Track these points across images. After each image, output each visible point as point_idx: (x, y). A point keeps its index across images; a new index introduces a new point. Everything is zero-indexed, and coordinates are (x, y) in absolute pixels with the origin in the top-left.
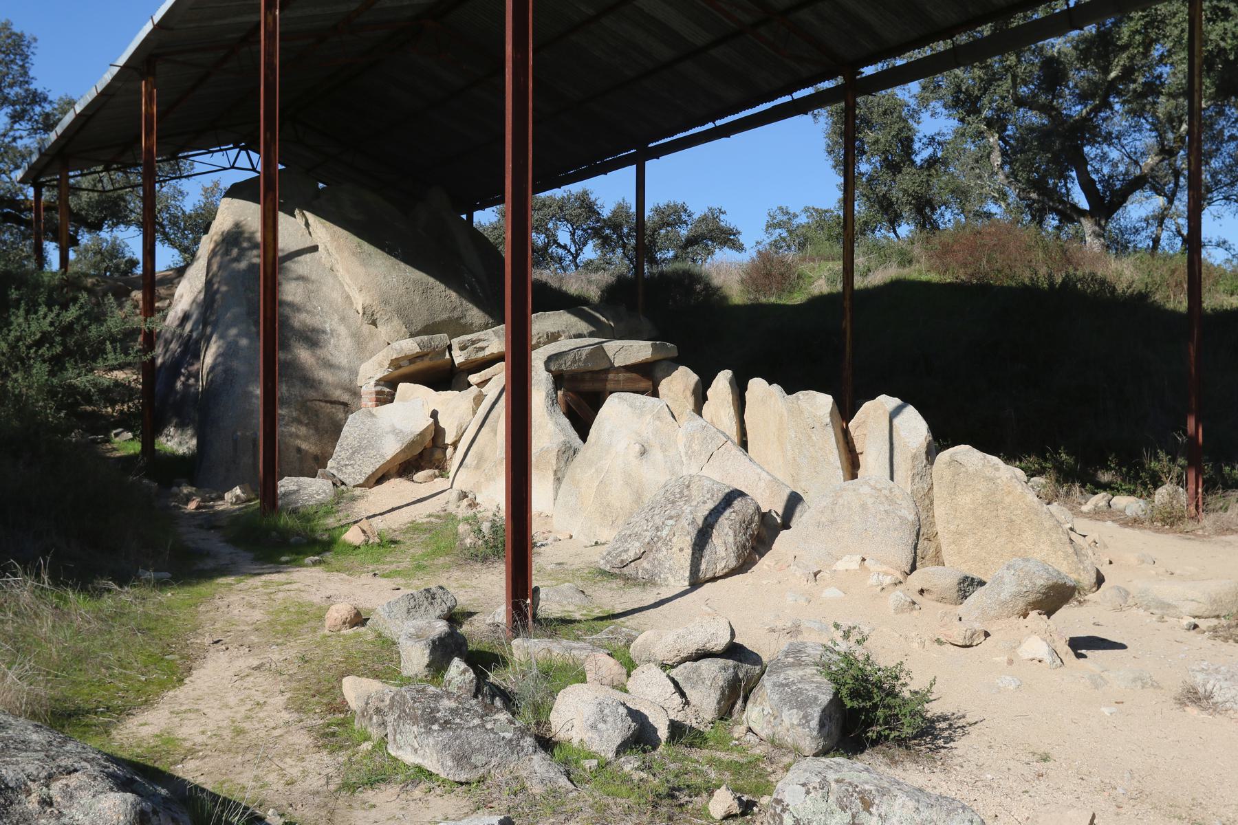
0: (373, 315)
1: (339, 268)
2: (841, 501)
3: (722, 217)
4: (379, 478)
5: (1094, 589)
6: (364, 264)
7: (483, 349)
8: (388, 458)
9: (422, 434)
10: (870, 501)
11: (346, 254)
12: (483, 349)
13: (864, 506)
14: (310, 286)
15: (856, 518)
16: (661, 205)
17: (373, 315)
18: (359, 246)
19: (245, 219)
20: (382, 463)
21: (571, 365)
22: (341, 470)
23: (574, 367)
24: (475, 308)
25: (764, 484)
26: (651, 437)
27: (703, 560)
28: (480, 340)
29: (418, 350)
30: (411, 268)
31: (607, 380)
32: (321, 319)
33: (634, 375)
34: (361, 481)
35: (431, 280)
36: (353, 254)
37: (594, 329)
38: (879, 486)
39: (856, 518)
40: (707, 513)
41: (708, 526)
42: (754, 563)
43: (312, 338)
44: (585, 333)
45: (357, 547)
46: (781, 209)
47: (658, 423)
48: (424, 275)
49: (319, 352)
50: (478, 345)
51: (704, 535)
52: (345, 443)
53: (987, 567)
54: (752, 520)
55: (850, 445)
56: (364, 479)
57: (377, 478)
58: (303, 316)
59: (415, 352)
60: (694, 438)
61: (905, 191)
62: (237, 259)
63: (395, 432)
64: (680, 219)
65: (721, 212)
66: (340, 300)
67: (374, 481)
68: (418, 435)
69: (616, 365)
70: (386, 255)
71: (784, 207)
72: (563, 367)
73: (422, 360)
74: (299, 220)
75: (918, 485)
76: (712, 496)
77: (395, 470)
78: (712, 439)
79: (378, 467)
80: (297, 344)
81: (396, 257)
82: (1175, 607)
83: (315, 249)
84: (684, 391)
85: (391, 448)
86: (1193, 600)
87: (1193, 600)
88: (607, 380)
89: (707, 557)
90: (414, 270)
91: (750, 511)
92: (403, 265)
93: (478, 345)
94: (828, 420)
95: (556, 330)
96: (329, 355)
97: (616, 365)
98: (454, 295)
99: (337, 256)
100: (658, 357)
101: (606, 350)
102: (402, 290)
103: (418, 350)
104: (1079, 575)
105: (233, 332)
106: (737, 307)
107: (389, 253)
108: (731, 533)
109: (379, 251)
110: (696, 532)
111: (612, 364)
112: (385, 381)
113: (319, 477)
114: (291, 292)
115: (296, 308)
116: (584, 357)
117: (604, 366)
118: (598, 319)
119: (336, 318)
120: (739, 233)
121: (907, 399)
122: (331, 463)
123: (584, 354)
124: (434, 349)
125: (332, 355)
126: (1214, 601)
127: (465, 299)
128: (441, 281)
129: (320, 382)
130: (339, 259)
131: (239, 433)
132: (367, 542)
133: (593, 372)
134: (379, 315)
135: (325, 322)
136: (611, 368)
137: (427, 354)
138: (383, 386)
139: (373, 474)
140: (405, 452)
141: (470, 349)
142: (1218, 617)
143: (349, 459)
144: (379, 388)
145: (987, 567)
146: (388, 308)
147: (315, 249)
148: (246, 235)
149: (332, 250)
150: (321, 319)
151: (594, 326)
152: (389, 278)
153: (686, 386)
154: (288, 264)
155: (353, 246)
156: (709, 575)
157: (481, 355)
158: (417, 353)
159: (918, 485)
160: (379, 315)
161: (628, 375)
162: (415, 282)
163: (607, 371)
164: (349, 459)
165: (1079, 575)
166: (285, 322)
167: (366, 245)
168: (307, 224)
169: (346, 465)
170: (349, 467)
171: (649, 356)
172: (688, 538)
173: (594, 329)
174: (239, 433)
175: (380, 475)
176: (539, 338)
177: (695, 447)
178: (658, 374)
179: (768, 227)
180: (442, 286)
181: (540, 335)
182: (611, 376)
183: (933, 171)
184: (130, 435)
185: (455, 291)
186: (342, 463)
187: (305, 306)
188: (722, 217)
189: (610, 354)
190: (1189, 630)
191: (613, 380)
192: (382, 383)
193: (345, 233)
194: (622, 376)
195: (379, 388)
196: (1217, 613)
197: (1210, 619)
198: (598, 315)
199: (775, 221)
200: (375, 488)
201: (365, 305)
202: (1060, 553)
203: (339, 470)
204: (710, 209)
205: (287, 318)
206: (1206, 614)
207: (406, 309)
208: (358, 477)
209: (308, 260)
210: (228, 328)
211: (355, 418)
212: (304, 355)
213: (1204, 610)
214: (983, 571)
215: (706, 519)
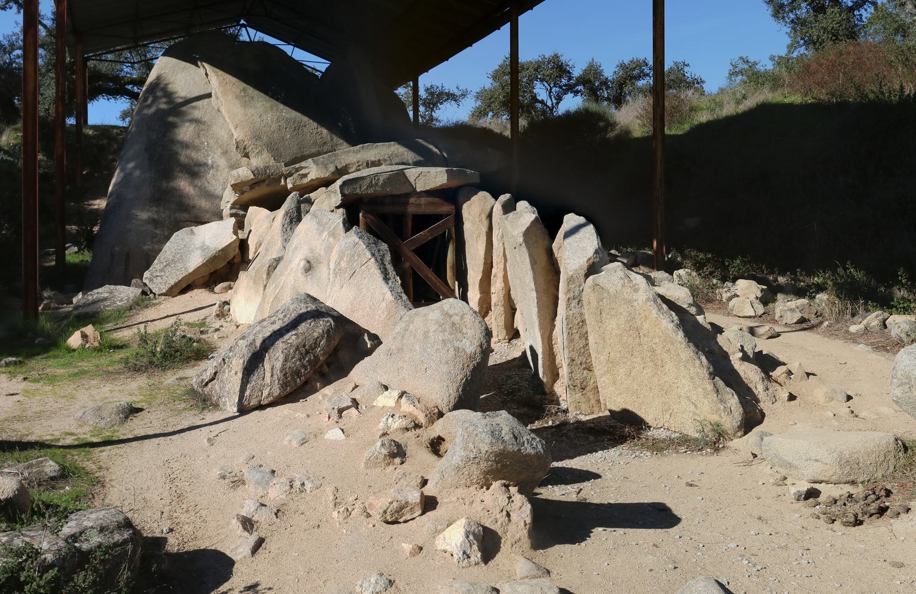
0: (245, 149)
1: (223, 110)
2: (411, 327)
3: (686, 69)
4: (184, 287)
5: (739, 434)
6: (245, 105)
7: (305, 175)
8: (191, 271)
9: (224, 250)
10: (433, 328)
11: (230, 97)
12: (305, 175)
13: (426, 334)
14: (201, 126)
15: (417, 348)
16: (626, 62)
17: (245, 149)
18: (244, 90)
19: (165, 73)
20: (184, 275)
21: (367, 189)
22: (152, 280)
23: (371, 191)
24: (345, 143)
25: (385, 305)
26: (322, 253)
27: (248, 386)
28: (302, 168)
29: (252, 177)
30: (288, 108)
31: (408, 204)
32: (206, 153)
33: (436, 199)
34: (164, 291)
35: (305, 119)
36: (237, 97)
37: (421, 159)
38: (451, 312)
39: (417, 348)
40: (268, 334)
41: (264, 348)
42: (314, 391)
43: (194, 171)
44: (410, 162)
45: (74, 350)
46: (741, 58)
47: (331, 239)
48: (299, 115)
49: (198, 182)
50: (301, 172)
51: (256, 359)
52: (163, 257)
53: (640, 401)
54: (316, 343)
55: (556, 266)
56: (167, 288)
57: (181, 289)
58: (188, 152)
59: (250, 178)
60: (344, 255)
61: (825, 29)
62: (149, 106)
63: (203, 248)
64: (642, 71)
65: (685, 65)
66: (226, 137)
67: (178, 291)
68: (220, 251)
69: (418, 190)
70: (267, 98)
71: (744, 57)
72: (358, 191)
73: (260, 186)
74: (202, 71)
75: (574, 311)
76: (285, 316)
77: (201, 281)
78: (359, 256)
79: (180, 278)
80: (180, 174)
81: (277, 100)
82: (796, 468)
83: (209, 96)
84: (480, 215)
85: (195, 261)
86: (817, 461)
87: (817, 461)
88: (408, 204)
89: (253, 383)
90: (291, 110)
91: (316, 335)
92: (281, 106)
93: (301, 172)
94: (521, 240)
95: (377, 159)
96: (206, 183)
97: (418, 190)
98: (325, 131)
99: (222, 99)
100: (455, 183)
101: (408, 176)
102: (274, 126)
103: (252, 177)
104: (721, 417)
105: (131, 165)
106: (637, 139)
107: (272, 97)
108: (281, 358)
109: (262, 94)
110: (250, 355)
111: (415, 189)
112: (241, 205)
113: (133, 286)
114: (185, 132)
115: (186, 146)
116: (381, 182)
117: (405, 190)
118: (430, 150)
119: (219, 151)
120: (703, 82)
121: (590, 220)
122: (147, 274)
123: (381, 179)
124: (269, 176)
125: (208, 183)
126: (844, 462)
127: (336, 135)
128: (314, 120)
129: (194, 207)
130: (224, 101)
131: (116, 248)
132: (83, 346)
133: (393, 196)
134: (250, 148)
135: (208, 155)
136: (414, 192)
137: (264, 181)
138: (238, 209)
139: (176, 284)
140: (207, 266)
141: (295, 175)
142: (853, 483)
143: (161, 271)
144: (234, 211)
145: (640, 401)
146: (259, 143)
147: (209, 96)
148: (161, 86)
149: (220, 95)
150: (206, 153)
151: (422, 156)
152: (264, 117)
153: (482, 210)
154: (184, 108)
155: (238, 91)
156: (254, 402)
157: (305, 181)
158: (252, 179)
159: (574, 311)
160: (250, 148)
161: (430, 199)
162: (288, 121)
163: (407, 196)
164: (161, 271)
165: (721, 417)
166: (174, 156)
167: (251, 91)
168: (207, 75)
169: (157, 276)
170: (159, 278)
171: (445, 182)
172: (242, 361)
173: (421, 159)
174: (116, 248)
175: (184, 286)
176: (359, 166)
177: (343, 264)
178: (461, 199)
179: (731, 75)
180: (315, 124)
181: (360, 163)
182: (412, 200)
183: (863, 10)
184: (76, 249)
185: (326, 129)
186: (155, 274)
187: (193, 142)
188: (686, 69)
189: (412, 179)
190: (798, 500)
191: (414, 204)
192: (238, 206)
193: (234, 80)
194: (423, 200)
195: (234, 211)
196: (851, 478)
197: (842, 486)
198: (431, 147)
199: (737, 70)
200: (178, 297)
201: (238, 140)
202: (700, 390)
203: (151, 280)
204: (676, 63)
205: (177, 153)
206: (834, 478)
207: (276, 143)
208: (162, 287)
209: (205, 104)
210: (128, 161)
211: (178, 236)
212: (183, 185)
213: (831, 473)
214: (637, 405)
215: (264, 341)
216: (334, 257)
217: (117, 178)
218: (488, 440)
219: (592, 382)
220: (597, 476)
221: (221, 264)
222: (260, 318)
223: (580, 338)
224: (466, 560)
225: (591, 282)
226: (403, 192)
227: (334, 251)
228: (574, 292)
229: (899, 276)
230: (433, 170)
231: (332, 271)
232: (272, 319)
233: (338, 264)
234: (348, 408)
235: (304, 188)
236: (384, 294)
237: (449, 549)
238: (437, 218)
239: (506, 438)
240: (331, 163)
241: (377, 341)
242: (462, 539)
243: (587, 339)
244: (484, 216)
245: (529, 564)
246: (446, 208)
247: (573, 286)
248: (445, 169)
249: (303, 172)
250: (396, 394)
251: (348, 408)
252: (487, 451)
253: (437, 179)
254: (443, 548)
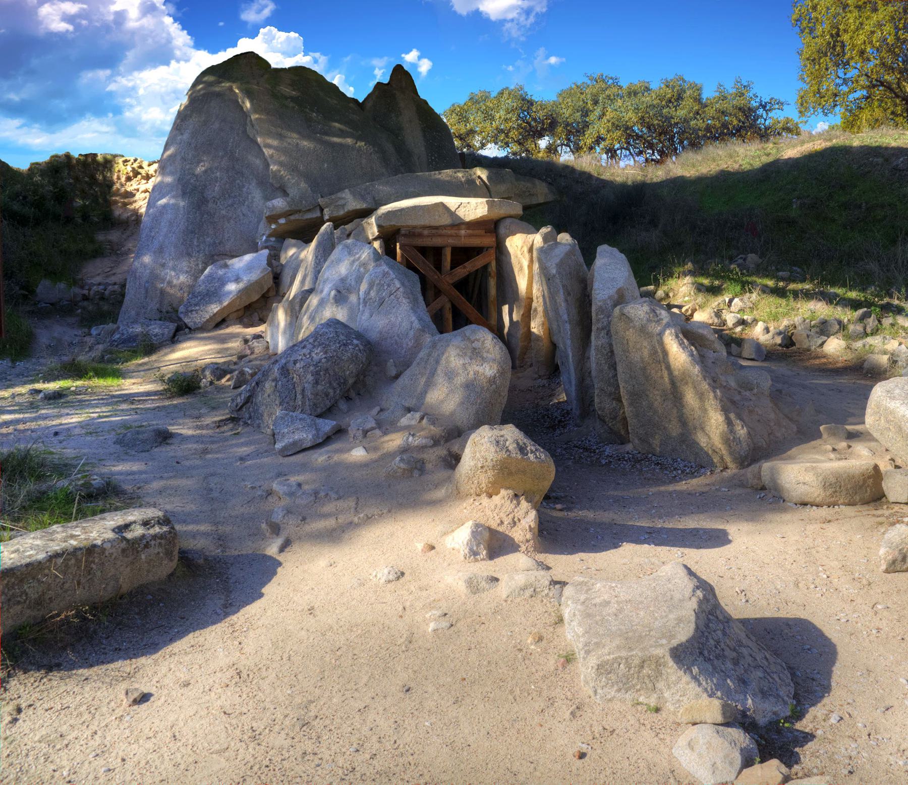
29: (288, 208)
66: (261, 167)
67: (214, 324)
153: (524, 242)
169: (192, 311)
171: (485, 213)
175: (219, 319)
177: (373, 294)
216: (364, 287)
217: (225, 362)
218: (493, 449)
219: (621, 412)
220: (685, 567)
221: (255, 297)
222: (291, 344)
223: (609, 368)
224: (472, 557)
225: (618, 311)
226: (442, 224)
227: (364, 280)
228: (603, 323)
229: (521, 158)
230: (473, 201)
231: (361, 301)
232: (303, 344)
233: (367, 293)
234: (372, 429)
235: (341, 219)
236: (412, 323)
237: (457, 546)
238: (478, 251)
239: (510, 448)
240: (369, 193)
241: (730, 542)
242: (468, 538)
243: (615, 370)
244: (526, 249)
245: (530, 560)
246: (489, 241)
247: (602, 316)
248: (485, 200)
249: (340, 203)
250: (418, 415)
251: (372, 429)
252: (492, 460)
253: (477, 211)
254: (452, 546)
